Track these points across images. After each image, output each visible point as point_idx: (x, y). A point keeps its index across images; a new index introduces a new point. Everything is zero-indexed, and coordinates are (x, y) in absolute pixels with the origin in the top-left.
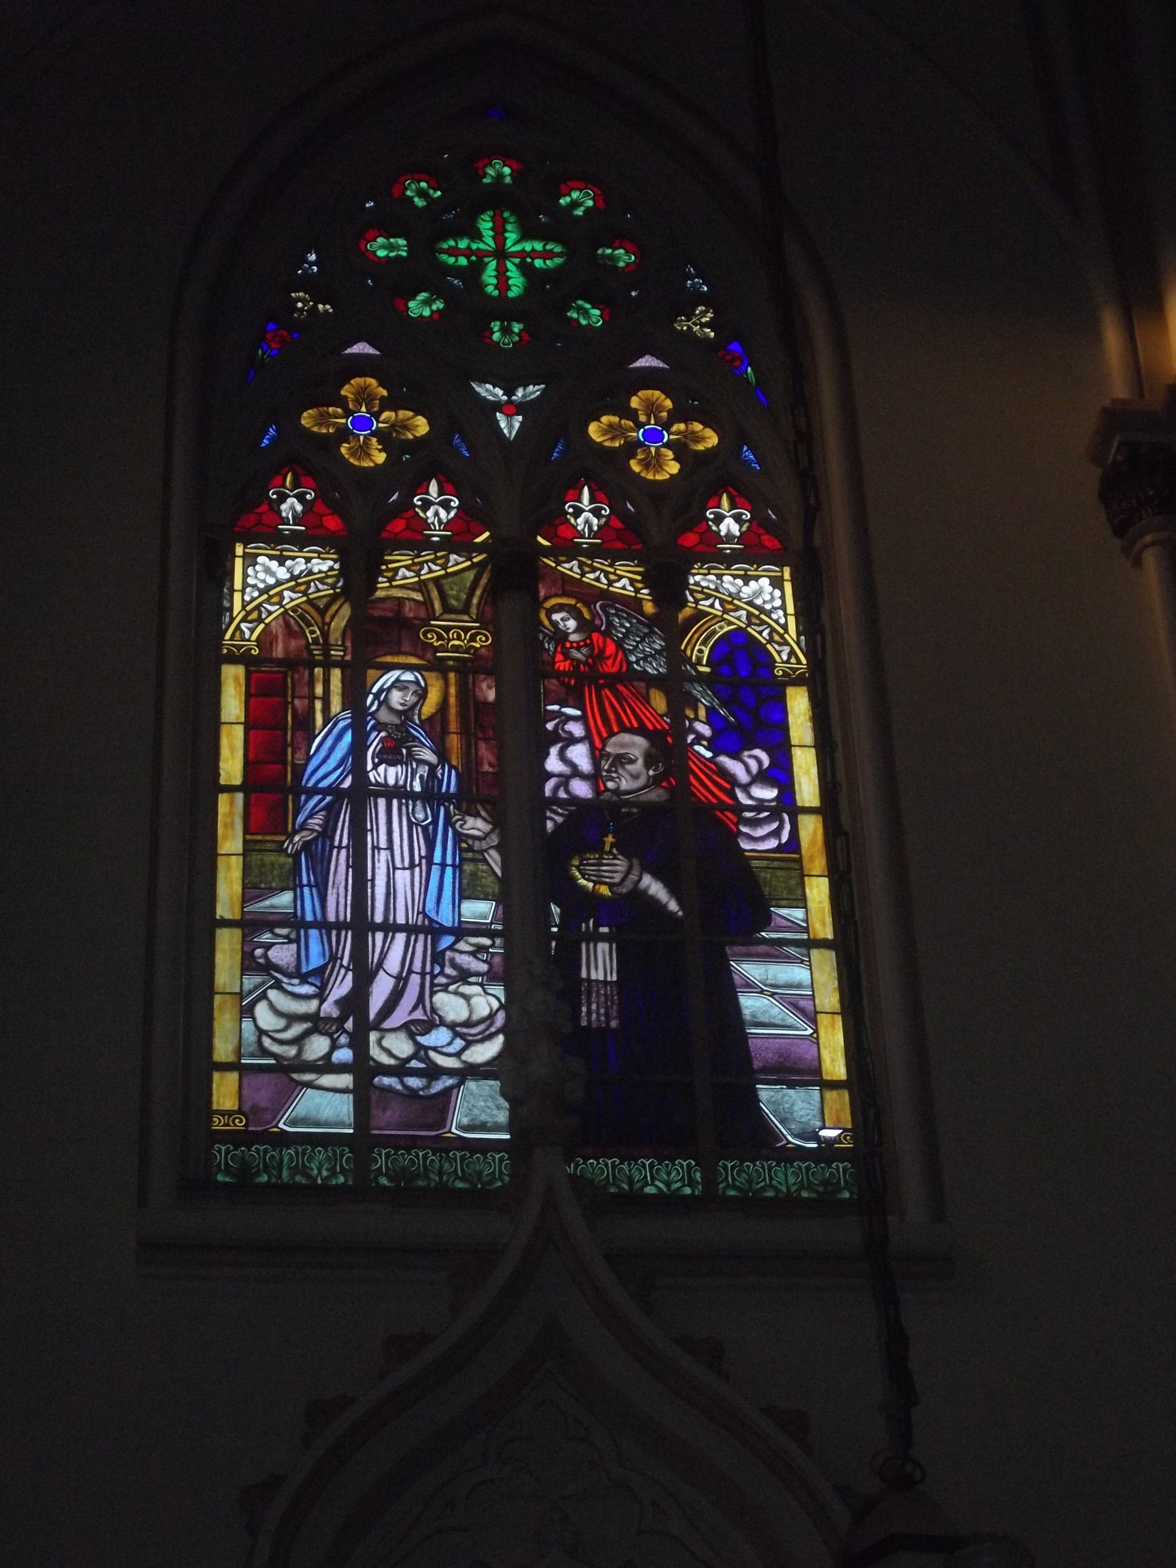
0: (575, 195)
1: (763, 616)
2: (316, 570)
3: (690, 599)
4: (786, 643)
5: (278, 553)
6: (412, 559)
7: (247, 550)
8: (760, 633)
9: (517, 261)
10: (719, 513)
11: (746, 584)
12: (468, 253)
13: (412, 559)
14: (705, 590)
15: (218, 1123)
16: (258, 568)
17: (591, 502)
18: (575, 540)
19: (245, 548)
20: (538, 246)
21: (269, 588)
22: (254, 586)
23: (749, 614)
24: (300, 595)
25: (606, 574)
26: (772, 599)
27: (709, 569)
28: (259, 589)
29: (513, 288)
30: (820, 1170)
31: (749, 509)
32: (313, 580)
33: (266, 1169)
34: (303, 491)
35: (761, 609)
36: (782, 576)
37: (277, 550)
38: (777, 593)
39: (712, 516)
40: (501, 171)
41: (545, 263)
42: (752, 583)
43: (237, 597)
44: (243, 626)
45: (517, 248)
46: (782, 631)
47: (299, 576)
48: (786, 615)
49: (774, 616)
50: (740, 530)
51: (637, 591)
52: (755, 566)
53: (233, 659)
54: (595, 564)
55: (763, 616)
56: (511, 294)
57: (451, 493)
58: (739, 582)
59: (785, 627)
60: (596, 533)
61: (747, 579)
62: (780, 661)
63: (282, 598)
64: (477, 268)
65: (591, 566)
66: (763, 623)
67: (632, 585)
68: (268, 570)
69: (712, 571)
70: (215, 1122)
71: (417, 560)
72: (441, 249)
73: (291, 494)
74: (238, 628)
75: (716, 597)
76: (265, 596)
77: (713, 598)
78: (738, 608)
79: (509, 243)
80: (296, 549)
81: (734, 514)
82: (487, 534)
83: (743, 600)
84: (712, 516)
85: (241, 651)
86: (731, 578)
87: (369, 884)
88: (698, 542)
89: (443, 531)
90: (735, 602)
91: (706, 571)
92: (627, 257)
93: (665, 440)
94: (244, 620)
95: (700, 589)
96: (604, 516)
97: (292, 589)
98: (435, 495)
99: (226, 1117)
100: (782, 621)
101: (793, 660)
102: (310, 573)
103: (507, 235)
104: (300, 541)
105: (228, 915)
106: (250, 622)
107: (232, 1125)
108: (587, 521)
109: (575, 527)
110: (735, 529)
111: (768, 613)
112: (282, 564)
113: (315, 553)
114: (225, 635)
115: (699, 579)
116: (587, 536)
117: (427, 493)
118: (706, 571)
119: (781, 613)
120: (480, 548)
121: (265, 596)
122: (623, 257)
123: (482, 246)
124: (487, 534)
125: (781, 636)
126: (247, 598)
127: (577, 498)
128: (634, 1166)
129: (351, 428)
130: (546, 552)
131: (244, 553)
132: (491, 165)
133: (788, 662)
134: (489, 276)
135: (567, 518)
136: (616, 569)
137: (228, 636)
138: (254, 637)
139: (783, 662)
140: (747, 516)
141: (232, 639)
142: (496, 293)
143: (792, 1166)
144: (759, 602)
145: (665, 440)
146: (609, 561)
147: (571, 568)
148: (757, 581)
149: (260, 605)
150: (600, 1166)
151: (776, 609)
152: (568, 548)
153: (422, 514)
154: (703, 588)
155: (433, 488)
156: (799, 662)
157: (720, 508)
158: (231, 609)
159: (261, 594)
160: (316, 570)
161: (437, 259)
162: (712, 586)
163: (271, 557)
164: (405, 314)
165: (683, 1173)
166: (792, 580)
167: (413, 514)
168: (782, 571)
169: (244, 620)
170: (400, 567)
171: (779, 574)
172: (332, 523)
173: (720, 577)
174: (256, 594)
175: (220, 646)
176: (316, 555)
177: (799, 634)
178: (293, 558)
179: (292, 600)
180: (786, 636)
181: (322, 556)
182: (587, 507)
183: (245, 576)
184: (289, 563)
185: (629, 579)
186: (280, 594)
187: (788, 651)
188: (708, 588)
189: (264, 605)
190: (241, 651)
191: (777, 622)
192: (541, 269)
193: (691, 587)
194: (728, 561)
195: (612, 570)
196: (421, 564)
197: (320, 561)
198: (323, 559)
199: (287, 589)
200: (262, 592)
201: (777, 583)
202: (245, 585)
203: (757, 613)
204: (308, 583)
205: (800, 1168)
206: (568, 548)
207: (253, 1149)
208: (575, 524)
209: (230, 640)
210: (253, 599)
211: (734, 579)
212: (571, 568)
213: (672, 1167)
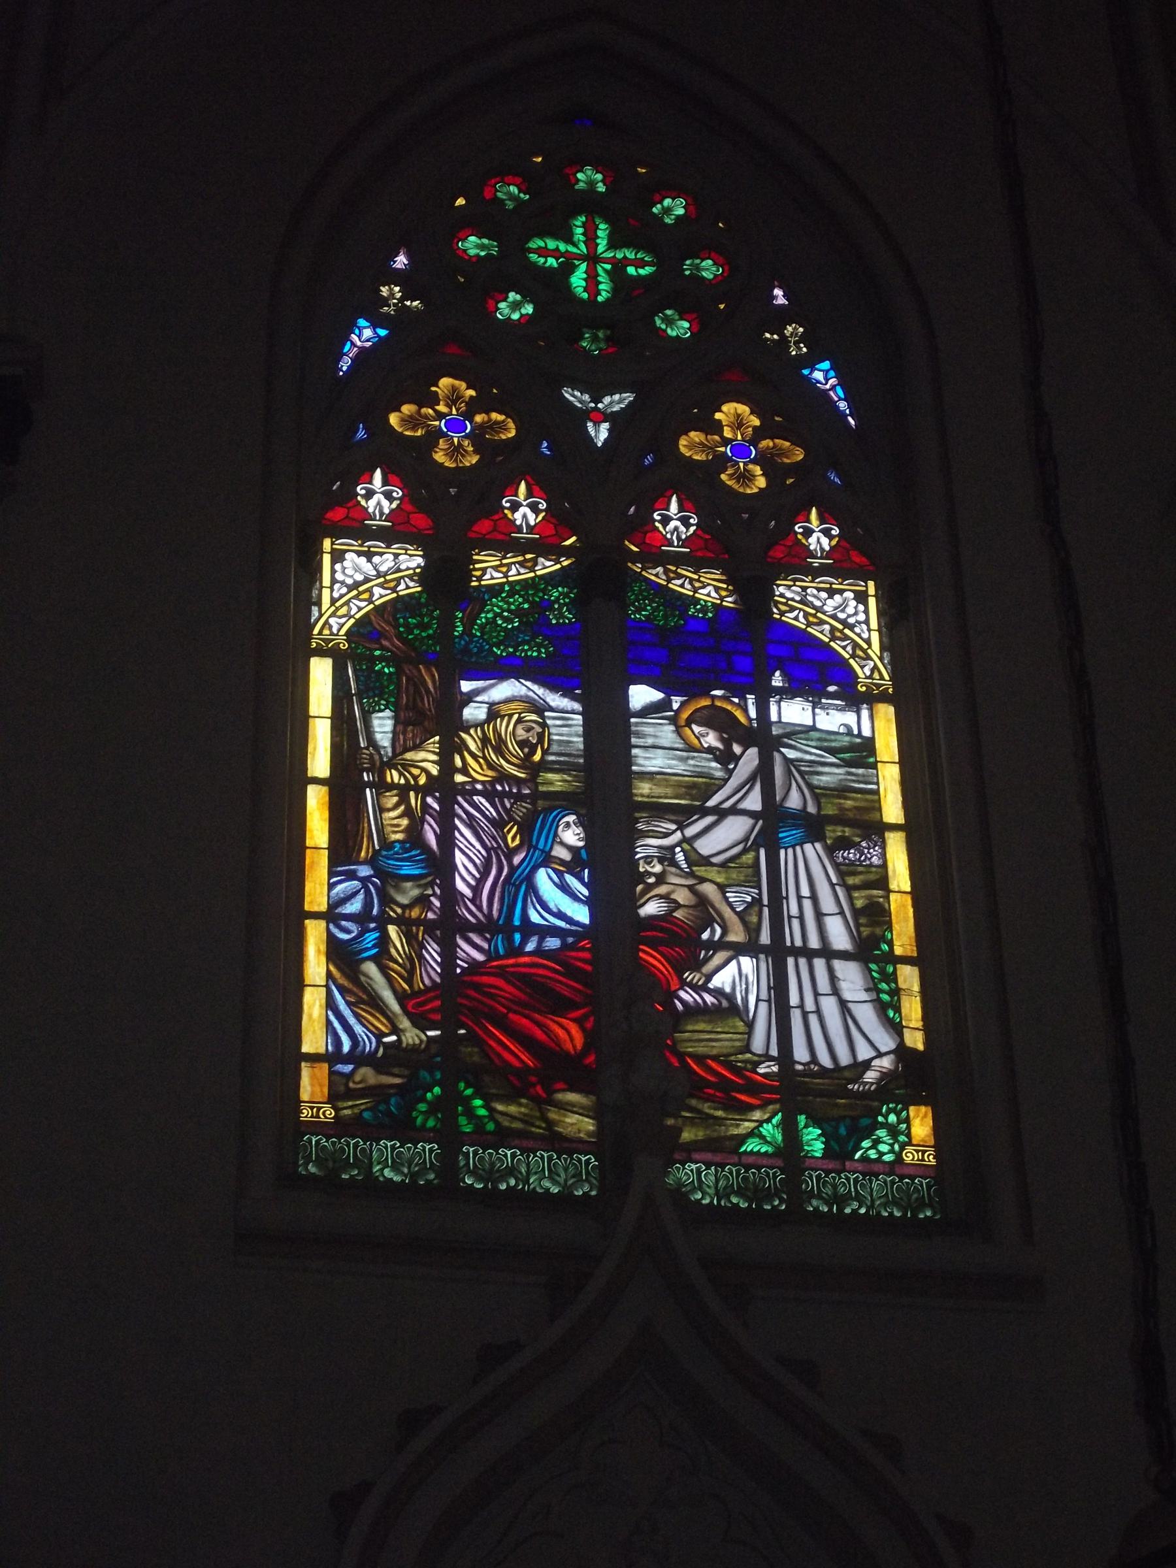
0: (667, 202)
1: (847, 631)
2: (403, 567)
3: (775, 610)
4: (869, 658)
5: (366, 549)
6: (500, 560)
7: (335, 546)
8: (844, 648)
9: (608, 267)
10: (808, 527)
11: (831, 597)
12: (556, 253)
13: (500, 560)
14: (790, 602)
15: (306, 1114)
16: (346, 563)
17: (385, 483)
18: (512, 535)
19: (333, 543)
20: (631, 255)
21: (357, 585)
22: (342, 583)
23: (833, 629)
24: (389, 592)
25: (691, 580)
26: (856, 614)
27: (794, 580)
28: (347, 586)
29: (604, 293)
30: (751, 1175)
31: (694, 511)
32: (402, 577)
33: (357, 1163)
34: (824, 528)
35: (844, 623)
36: (867, 591)
37: (366, 546)
38: (861, 607)
39: (508, 505)
40: (588, 177)
41: (636, 271)
42: (837, 597)
43: (326, 594)
44: (332, 621)
45: (610, 255)
46: (865, 646)
47: (386, 574)
48: (869, 630)
49: (857, 630)
50: (829, 545)
51: (722, 599)
52: (360, 542)
53: (321, 652)
54: (679, 570)
55: (847, 631)
56: (600, 299)
57: (691, 511)
58: (824, 595)
59: (868, 642)
60: (684, 541)
61: (832, 593)
62: (864, 677)
63: (372, 595)
64: (568, 268)
65: (675, 572)
66: (846, 638)
67: (717, 591)
68: (357, 569)
69: (797, 583)
70: (303, 1113)
71: (505, 561)
72: (529, 248)
73: (675, 517)
74: (326, 622)
75: (801, 610)
76: (355, 592)
77: (798, 611)
78: (822, 622)
79: (601, 249)
80: (384, 546)
81: (383, 491)
82: (574, 539)
83: (827, 614)
84: (801, 530)
85: (330, 646)
86: (815, 592)
87: (785, 901)
88: (491, 529)
89: (384, 521)
90: (819, 615)
91: (791, 583)
92: (714, 269)
93: (443, 421)
94: (333, 615)
95: (784, 600)
96: (396, 499)
97: (381, 585)
98: (380, 486)
99: (920, 1154)
100: (865, 636)
101: (876, 675)
102: (399, 570)
103: (598, 241)
104: (389, 536)
105: (316, 909)
106: (340, 617)
107: (322, 1117)
108: (525, 516)
109: (366, 509)
110: (532, 519)
111: (851, 627)
112: (369, 560)
113: (827, 583)
114: (313, 630)
115: (784, 590)
116: (819, 555)
117: (516, 495)
118: (791, 583)
119: (864, 627)
120: (568, 552)
121: (355, 592)
122: (709, 269)
123: (571, 249)
124: (574, 539)
125: (864, 651)
126: (336, 595)
127: (806, 519)
128: (839, 1180)
129: (730, 455)
130: (635, 558)
131: (332, 548)
132: (582, 172)
133: (870, 677)
134: (578, 280)
135: (504, 513)
136: (700, 576)
137: (316, 631)
138: (343, 632)
139: (867, 678)
140: (398, 494)
141: (320, 633)
142: (585, 296)
143: (877, 1180)
144: (842, 616)
145: (443, 421)
146: (503, 553)
147: (656, 575)
148: (842, 595)
149: (349, 601)
150: (724, 1173)
151: (859, 623)
152: (655, 555)
153: (510, 516)
154: (788, 599)
155: (378, 475)
156: (882, 678)
157: (669, 511)
158: (319, 604)
159: (350, 590)
160: (403, 567)
161: (528, 259)
162: (798, 598)
163: (359, 554)
164: (494, 314)
165: (693, 1178)
166: (876, 596)
167: (502, 516)
168: (866, 586)
169: (333, 615)
170: (487, 568)
171: (864, 589)
172: (421, 521)
173: (804, 589)
174: (344, 590)
175: (310, 636)
176: (404, 552)
177: (883, 648)
178: (381, 554)
179: (381, 596)
180: (869, 651)
181: (409, 552)
182: (380, 489)
183: (333, 572)
184: (376, 559)
185: (715, 586)
186: (370, 590)
187: (872, 666)
188: (793, 600)
189: (352, 600)
190: (330, 646)
191: (859, 635)
192: (632, 276)
193: (776, 598)
194: (815, 573)
195: (696, 577)
196: (509, 565)
197: (407, 557)
198: (411, 556)
199: (376, 585)
200: (351, 588)
201: (861, 597)
202: (334, 581)
203: (840, 627)
204: (398, 580)
205: (885, 1182)
206: (655, 555)
207: (418, 1146)
208: (807, 544)
209: (319, 634)
210: (342, 596)
211: (819, 592)
212: (656, 575)
213: (839, 1180)
